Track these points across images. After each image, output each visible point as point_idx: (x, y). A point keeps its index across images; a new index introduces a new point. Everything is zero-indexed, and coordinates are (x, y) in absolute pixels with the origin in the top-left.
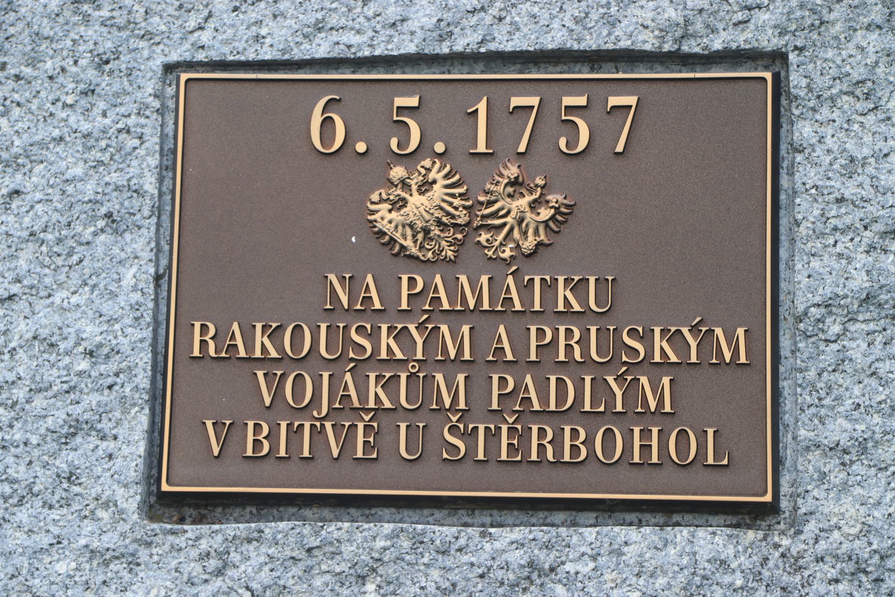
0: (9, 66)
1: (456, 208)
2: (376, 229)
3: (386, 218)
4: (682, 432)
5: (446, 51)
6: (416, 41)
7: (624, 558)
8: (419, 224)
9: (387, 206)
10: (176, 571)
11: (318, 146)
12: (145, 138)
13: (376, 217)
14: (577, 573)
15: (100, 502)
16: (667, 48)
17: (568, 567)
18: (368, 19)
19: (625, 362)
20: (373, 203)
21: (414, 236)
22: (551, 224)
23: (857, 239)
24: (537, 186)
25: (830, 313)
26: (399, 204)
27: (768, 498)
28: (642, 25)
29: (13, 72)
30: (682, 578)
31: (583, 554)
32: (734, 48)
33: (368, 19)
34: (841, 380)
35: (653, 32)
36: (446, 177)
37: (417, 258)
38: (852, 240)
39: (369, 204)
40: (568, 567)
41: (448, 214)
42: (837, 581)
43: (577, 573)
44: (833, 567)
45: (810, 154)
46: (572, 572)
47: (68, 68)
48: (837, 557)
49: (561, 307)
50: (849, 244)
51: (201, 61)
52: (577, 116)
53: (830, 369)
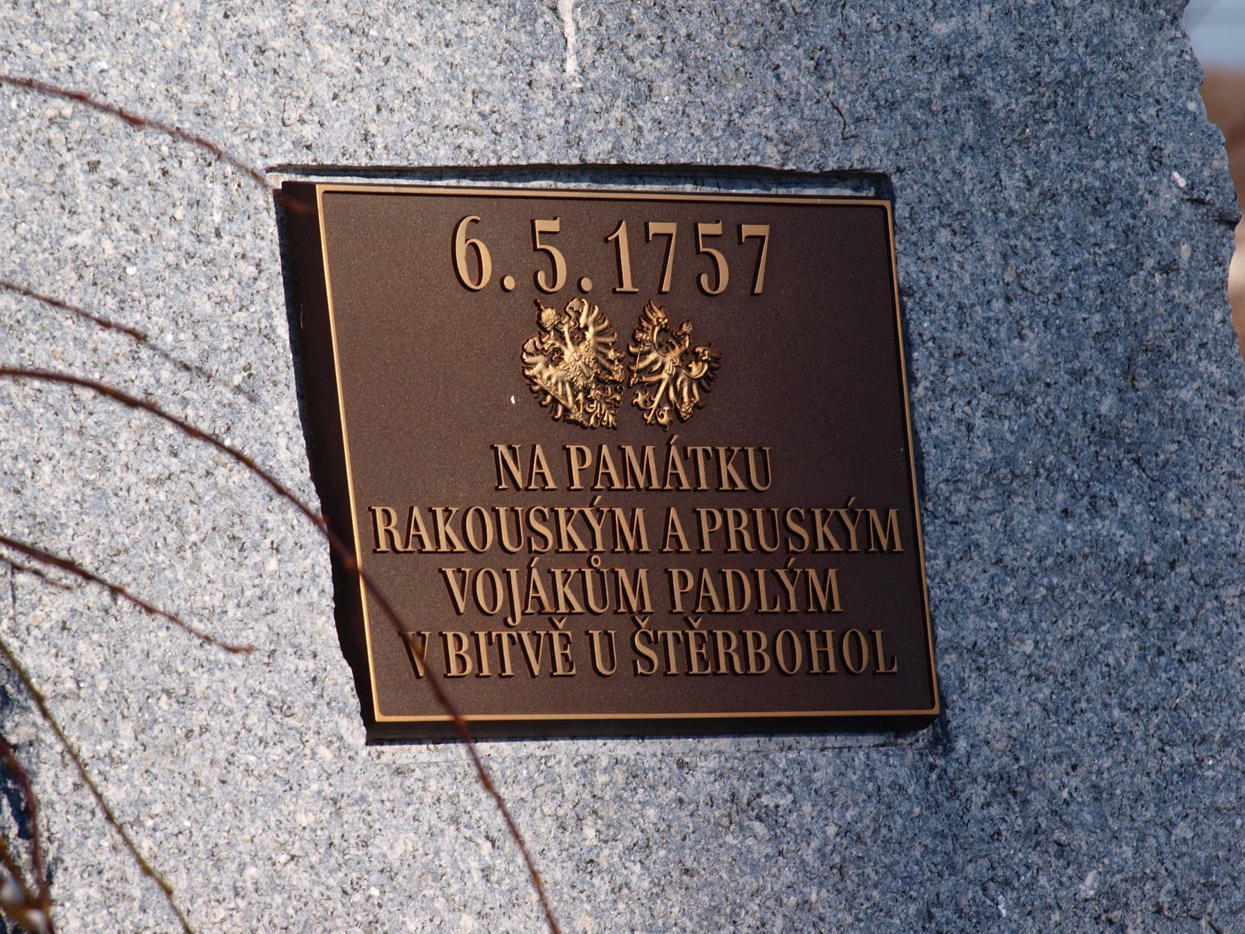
0: (101, 167)
1: (612, 362)
2: (537, 388)
3: (545, 374)
4: (788, 635)
5: (576, 161)
6: (546, 148)
7: (814, 787)
8: (580, 383)
9: (540, 359)
10: (415, 819)
11: (545, 288)
12: (264, 266)
13: (534, 371)
14: (777, 807)
15: (321, 736)
16: (790, 166)
17: (765, 800)
18: (483, 116)
19: (793, 552)
20: (529, 354)
21: (575, 396)
22: (703, 382)
23: (975, 402)
24: (685, 334)
25: (958, 490)
26: (555, 357)
27: (936, 710)
28: (766, 137)
29: (108, 174)
30: (871, 808)
31: (779, 784)
32: (847, 168)
33: (483, 116)
34: (968, 570)
35: (776, 146)
36: (595, 322)
37: (581, 424)
38: (969, 403)
39: (524, 356)
40: (765, 800)
41: (604, 368)
42: (989, 804)
43: (777, 807)
44: (984, 788)
45: (921, 299)
46: (772, 805)
47: (172, 171)
48: (988, 777)
49: (726, 486)
50: (967, 409)
51: (308, 166)
52: (718, 249)
53: (958, 557)
